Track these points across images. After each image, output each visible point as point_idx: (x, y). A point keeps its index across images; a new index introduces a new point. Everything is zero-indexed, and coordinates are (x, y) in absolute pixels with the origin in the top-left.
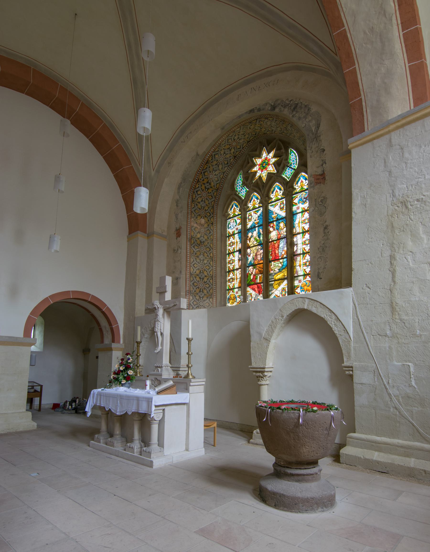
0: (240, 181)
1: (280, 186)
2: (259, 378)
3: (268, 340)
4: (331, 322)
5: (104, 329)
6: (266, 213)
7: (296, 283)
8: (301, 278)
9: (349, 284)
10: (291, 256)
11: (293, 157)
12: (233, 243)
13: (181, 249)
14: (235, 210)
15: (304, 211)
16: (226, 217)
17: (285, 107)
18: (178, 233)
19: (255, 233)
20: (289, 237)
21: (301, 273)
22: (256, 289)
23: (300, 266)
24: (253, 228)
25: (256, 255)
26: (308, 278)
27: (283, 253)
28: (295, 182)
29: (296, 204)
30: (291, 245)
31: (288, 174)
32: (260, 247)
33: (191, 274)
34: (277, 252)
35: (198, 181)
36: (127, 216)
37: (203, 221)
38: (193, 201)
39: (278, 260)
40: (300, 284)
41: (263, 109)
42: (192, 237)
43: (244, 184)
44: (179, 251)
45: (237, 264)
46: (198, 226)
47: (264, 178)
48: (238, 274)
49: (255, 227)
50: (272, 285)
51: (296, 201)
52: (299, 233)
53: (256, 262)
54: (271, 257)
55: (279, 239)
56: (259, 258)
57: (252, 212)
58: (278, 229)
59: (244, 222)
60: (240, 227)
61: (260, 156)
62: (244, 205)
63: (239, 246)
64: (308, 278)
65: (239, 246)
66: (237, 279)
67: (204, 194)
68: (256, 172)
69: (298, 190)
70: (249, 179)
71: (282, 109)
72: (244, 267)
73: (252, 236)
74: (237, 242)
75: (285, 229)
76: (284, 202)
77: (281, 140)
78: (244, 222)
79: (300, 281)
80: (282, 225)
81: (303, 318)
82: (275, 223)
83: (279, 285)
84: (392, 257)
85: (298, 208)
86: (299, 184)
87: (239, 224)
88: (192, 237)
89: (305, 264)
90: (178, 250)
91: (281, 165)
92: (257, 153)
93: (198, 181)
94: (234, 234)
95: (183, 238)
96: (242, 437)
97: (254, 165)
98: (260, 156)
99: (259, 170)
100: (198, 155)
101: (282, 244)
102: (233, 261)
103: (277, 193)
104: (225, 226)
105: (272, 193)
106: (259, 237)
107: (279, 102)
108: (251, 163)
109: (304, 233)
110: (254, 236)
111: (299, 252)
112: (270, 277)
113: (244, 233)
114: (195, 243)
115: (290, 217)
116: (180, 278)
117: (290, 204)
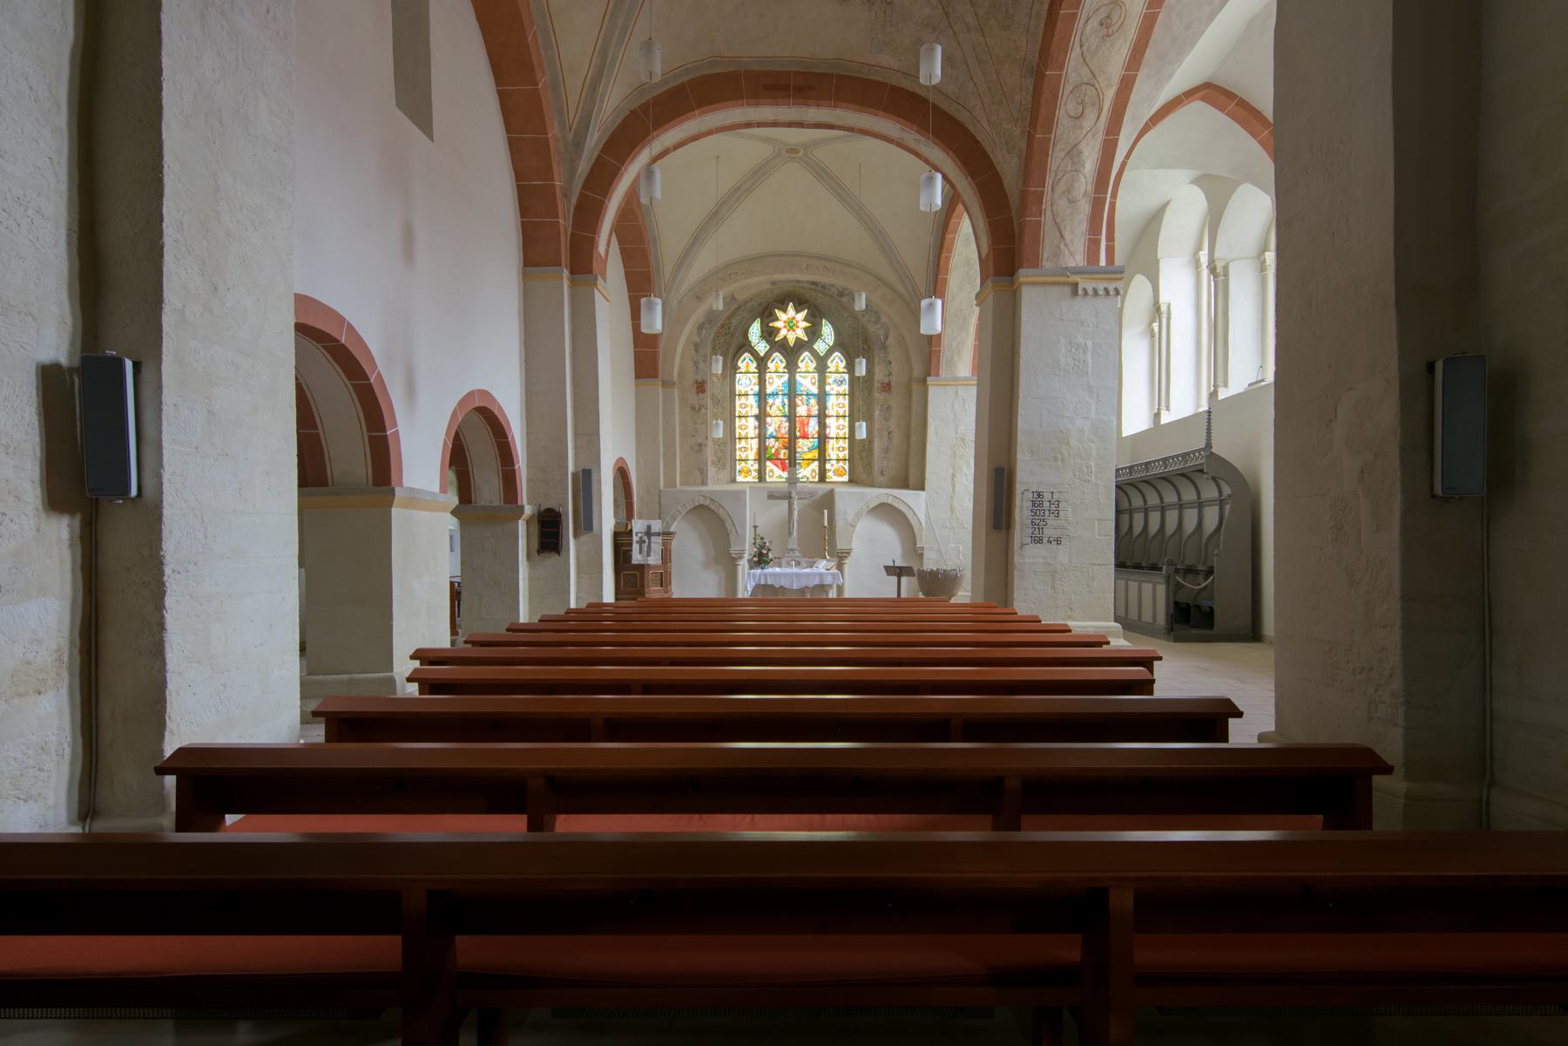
3: (853, 526)
4: (910, 516)
6: (792, 384)
7: (828, 466)
9: (923, 489)
10: (823, 438)
14: (746, 363)
15: (838, 394)
21: (833, 456)
24: (775, 394)
30: (822, 426)
36: (343, 319)
47: (791, 342)
48: (755, 444)
55: (809, 416)
59: (762, 382)
61: (806, 329)
62: (762, 363)
63: (755, 411)
70: (769, 334)
72: (762, 437)
78: (762, 382)
80: (813, 401)
81: (885, 511)
84: (953, 476)
96: (76, 806)
101: (813, 423)
103: (806, 362)
110: (777, 406)
115: (822, 397)
117: (822, 383)
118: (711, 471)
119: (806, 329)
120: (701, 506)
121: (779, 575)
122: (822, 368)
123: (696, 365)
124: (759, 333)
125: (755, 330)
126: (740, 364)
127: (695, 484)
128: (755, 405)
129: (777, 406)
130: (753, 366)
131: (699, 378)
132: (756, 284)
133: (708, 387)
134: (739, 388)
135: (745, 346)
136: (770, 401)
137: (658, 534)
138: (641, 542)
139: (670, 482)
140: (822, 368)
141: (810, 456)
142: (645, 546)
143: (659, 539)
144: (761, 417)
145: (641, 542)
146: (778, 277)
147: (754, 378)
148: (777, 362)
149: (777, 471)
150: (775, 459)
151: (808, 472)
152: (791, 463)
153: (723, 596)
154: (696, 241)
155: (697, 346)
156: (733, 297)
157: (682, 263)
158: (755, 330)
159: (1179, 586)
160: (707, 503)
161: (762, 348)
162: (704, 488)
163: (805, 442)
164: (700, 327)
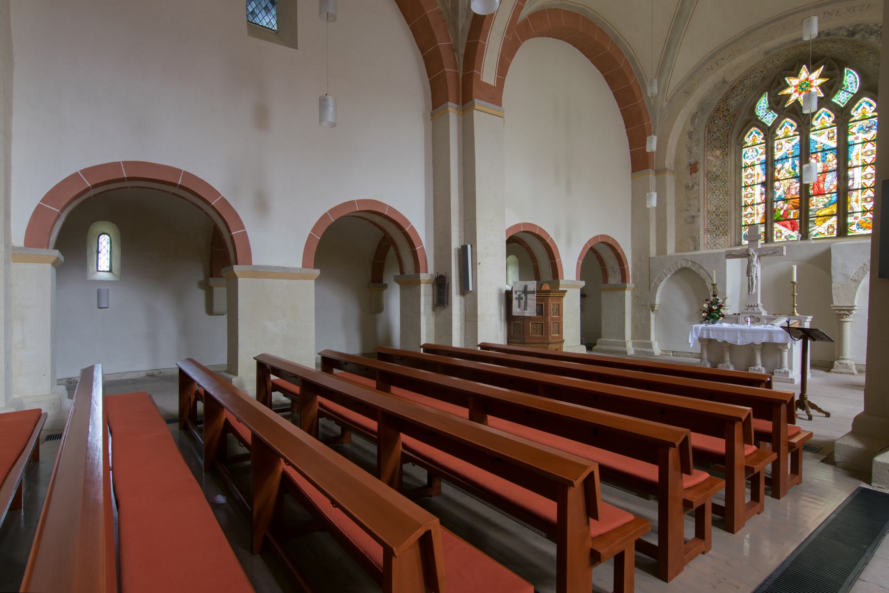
0: (763, 103)
1: (829, 112)
2: (841, 316)
5: (610, 271)
7: (850, 220)
8: (859, 215)
11: (851, 80)
12: (752, 176)
13: (699, 185)
14: (754, 137)
15: (865, 142)
16: (741, 144)
17: (871, 34)
18: (693, 168)
19: (788, 165)
20: (842, 169)
22: (789, 226)
23: (857, 201)
25: (789, 189)
26: (869, 215)
27: (832, 187)
28: (854, 109)
29: (853, 134)
31: (841, 98)
32: (794, 180)
33: (708, 212)
34: (821, 186)
35: (718, 110)
37: (718, 152)
38: (709, 131)
39: (824, 194)
40: (857, 221)
41: (835, 34)
42: (709, 172)
43: (771, 108)
44: (696, 188)
45: (758, 198)
46: (713, 160)
48: (761, 209)
49: (787, 158)
50: (813, 221)
51: (854, 130)
52: (857, 166)
53: (789, 197)
54: (811, 192)
55: (825, 172)
56: (793, 192)
57: (783, 141)
58: (823, 161)
59: (769, 151)
60: (763, 157)
62: (769, 133)
64: (869, 215)
65: (763, 178)
66: (758, 214)
67: (720, 123)
68: (789, 96)
69: (857, 118)
70: (777, 103)
71: (867, 36)
72: (769, 202)
73: (782, 168)
74: (758, 174)
75: (835, 161)
76: (835, 131)
77: (833, 59)
78: (769, 151)
79: (856, 218)
80: (830, 156)
82: (819, 154)
83: (824, 221)
85: (857, 138)
86: (859, 111)
87: (761, 154)
88: (709, 172)
89: (865, 200)
90: (693, 187)
91: (832, 86)
92: (795, 72)
93: (718, 110)
94: (753, 165)
95: (701, 173)
97: (787, 86)
98: (796, 75)
99: (795, 92)
100: (724, 81)
102: (752, 195)
104: (739, 156)
105: (817, 119)
106: (794, 168)
107: (862, 27)
108: (783, 85)
109: (864, 166)
111: (855, 187)
112: (810, 213)
113: (770, 164)
114: (712, 177)
115: (843, 151)
116: (698, 216)
118: (704, 238)
119: (821, 86)
120: (684, 269)
121: (724, 330)
122: (843, 117)
123: (690, 151)
124: (766, 106)
125: (763, 109)
126: (746, 139)
127: (689, 251)
128: (761, 173)
129: (785, 170)
130: (760, 138)
131: (692, 161)
132: (746, 59)
133: (701, 167)
134: (746, 161)
135: (753, 121)
136: (779, 166)
137: (533, 292)
138: (519, 298)
139: (662, 250)
140: (843, 117)
141: (826, 211)
142: (522, 302)
143: (534, 296)
144: (769, 184)
145: (519, 298)
146: (769, 45)
147: (761, 149)
148: (788, 127)
149: (786, 232)
150: (784, 220)
151: (823, 229)
152: (803, 225)
153: (463, 347)
154: (671, 44)
155: (690, 135)
156: (724, 81)
157: (663, 68)
158: (763, 103)
159: (652, 531)
160: (689, 265)
161: (769, 119)
162: (697, 253)
163: (820, 198)
164: (694, 117)
